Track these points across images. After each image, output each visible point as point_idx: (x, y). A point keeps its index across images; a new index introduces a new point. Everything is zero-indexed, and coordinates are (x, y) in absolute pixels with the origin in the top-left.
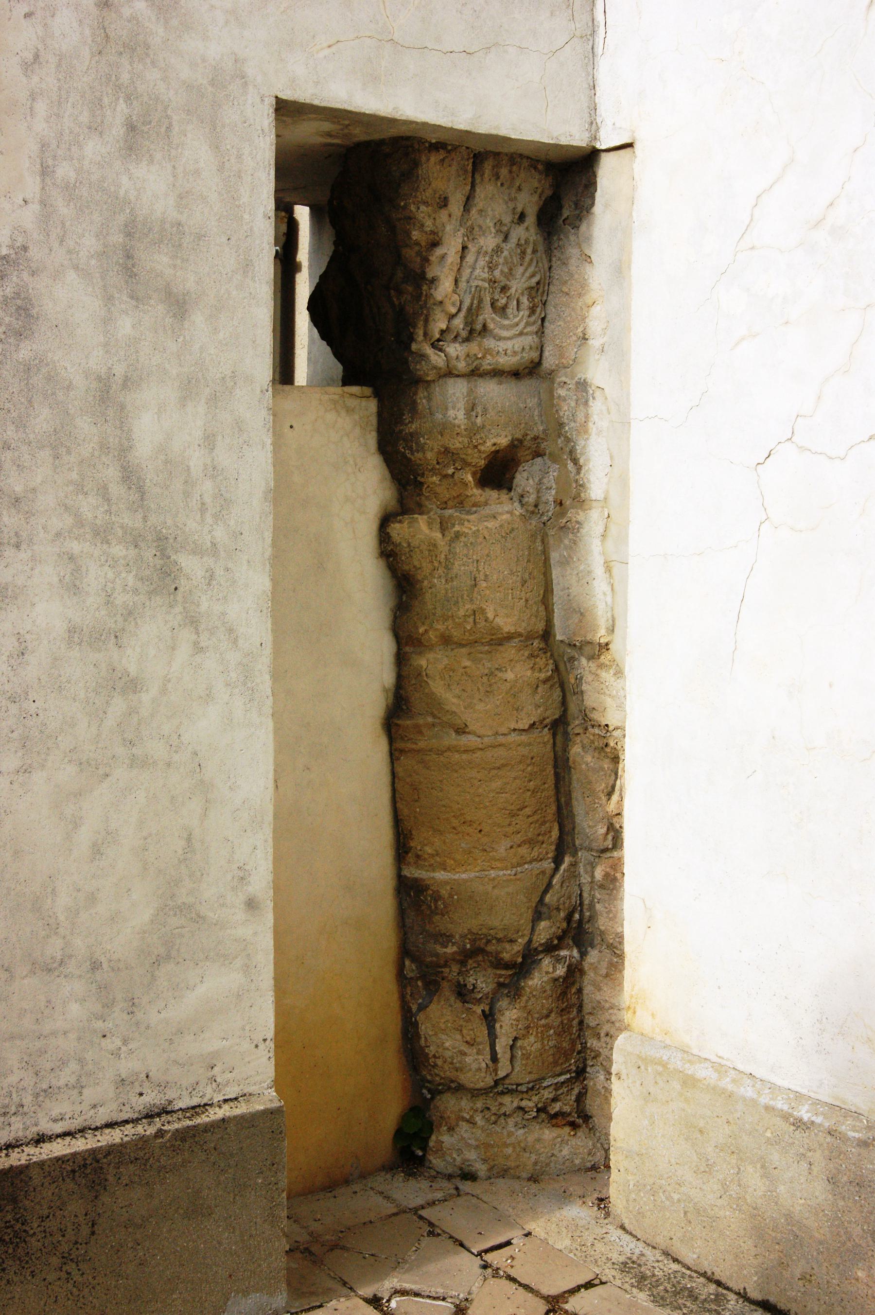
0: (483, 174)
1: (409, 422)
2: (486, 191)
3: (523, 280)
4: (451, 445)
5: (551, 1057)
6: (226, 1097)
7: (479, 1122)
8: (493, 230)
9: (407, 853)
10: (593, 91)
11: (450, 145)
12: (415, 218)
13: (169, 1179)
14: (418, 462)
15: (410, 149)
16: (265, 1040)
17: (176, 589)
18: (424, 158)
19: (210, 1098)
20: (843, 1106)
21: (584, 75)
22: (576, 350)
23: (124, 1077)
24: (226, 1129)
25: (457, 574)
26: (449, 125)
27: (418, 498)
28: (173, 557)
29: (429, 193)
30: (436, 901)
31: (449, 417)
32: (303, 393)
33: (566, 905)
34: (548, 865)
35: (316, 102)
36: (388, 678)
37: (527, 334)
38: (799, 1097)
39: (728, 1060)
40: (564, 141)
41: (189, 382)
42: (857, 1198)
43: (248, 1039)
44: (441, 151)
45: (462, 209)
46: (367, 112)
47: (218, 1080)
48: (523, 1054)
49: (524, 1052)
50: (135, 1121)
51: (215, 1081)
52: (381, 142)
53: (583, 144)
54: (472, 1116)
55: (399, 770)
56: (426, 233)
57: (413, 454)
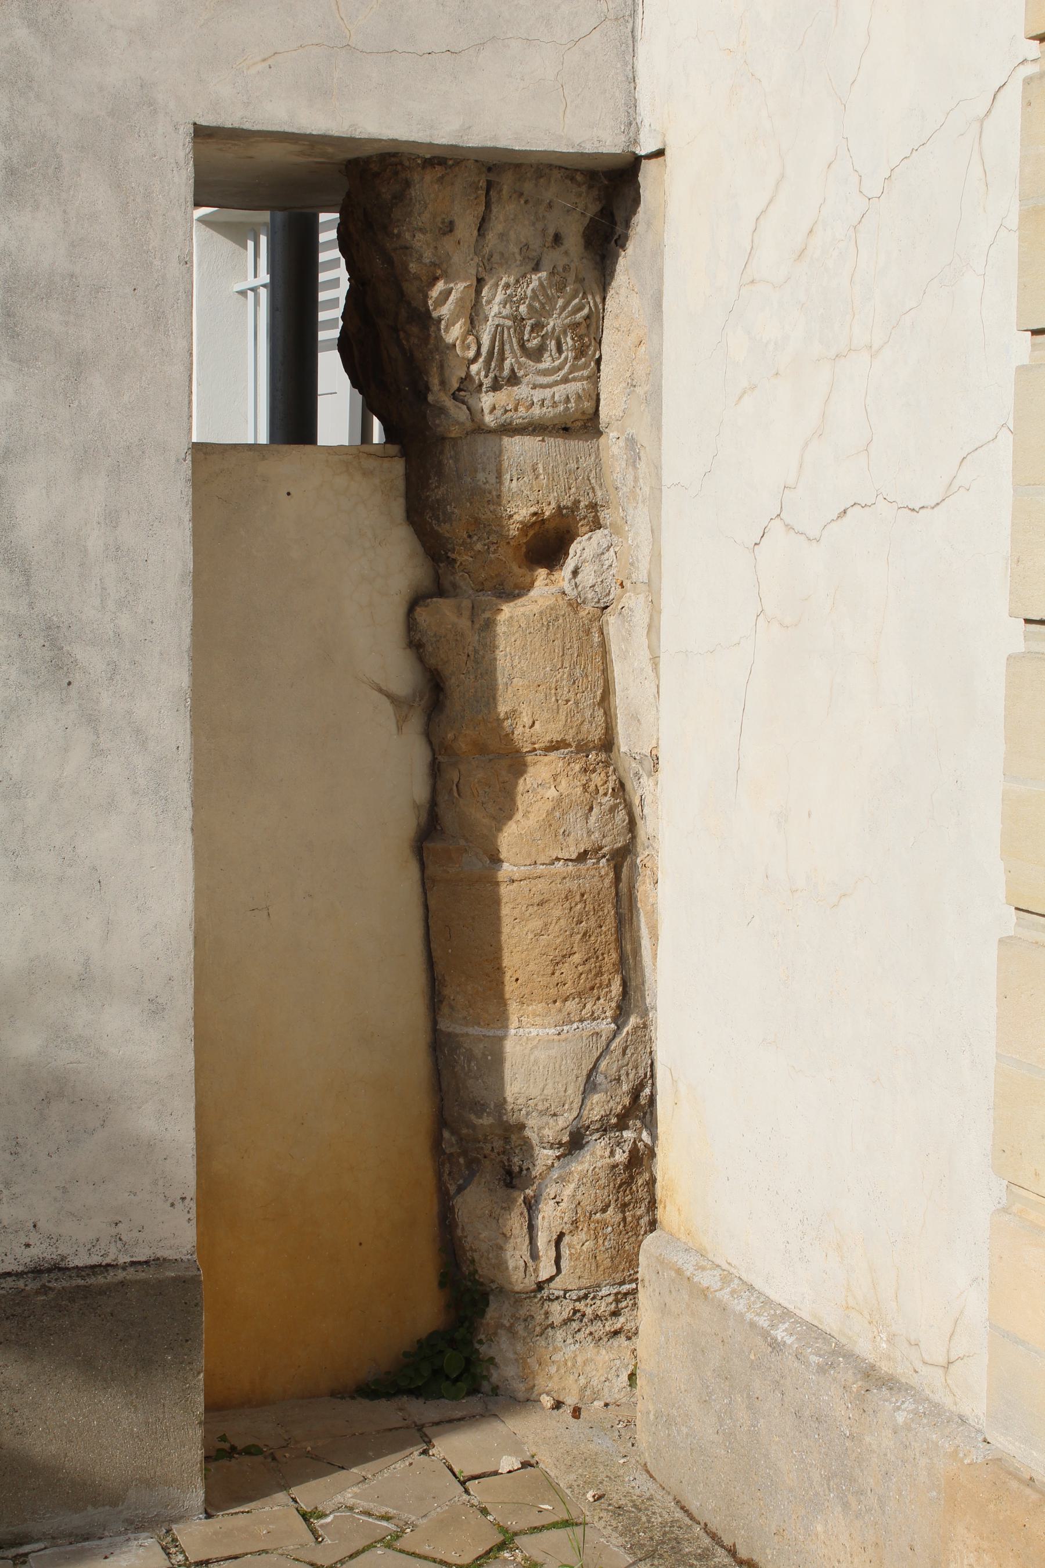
0: (501, 190)
1: (436, 487)
2: (503, 214)
3: (563, 315)
4: (480, 515)
5: (609, 1260)
6: (134, 1259)
7: (520, 1332)
8: (518, 257)
9: (441, 1002)
10: (632, 85)
11: (451, 159)
12: (412, 248)
13: (53, 1342)
14: (447, 535)
15: (399, 167)
16: (183, 1199)
17: (69, 683)
18: (416, 177)
19: (113, 1258)
20: (820, 1327)
21: (619, 65)
22: (625, 399)
23: (6, 1224)
24: (126, 1293)
25: (487, 670)
26: (427, 140)
27: (452, 578)
28: (67, 648)
29: (426, 216)
30: (469, 1062)
31: (479, 480)
32: (304, 454)
33: (631, 1076)
34: (606, 1026)
35: (247, 126)
36: (420, 792)
37: (574, 379)
38: (786, 1314)
39: (735, 1267)
40: (589, 148)
41: (86, 452)
42: (816, 1436)
43: (162, 1196)
44: (438, 168)
45: (476, 233)
46: (314, 133)
47: (124, 1239)
48: (571, 1254)
49: (573, 1251)
50: (19, 1275)
51: (120, 1239)
52: (368, 160)
53: (618, 150)
54: (512, 1325)
55: (432, 903)
56: (425, 265)
57: (439, 525)
